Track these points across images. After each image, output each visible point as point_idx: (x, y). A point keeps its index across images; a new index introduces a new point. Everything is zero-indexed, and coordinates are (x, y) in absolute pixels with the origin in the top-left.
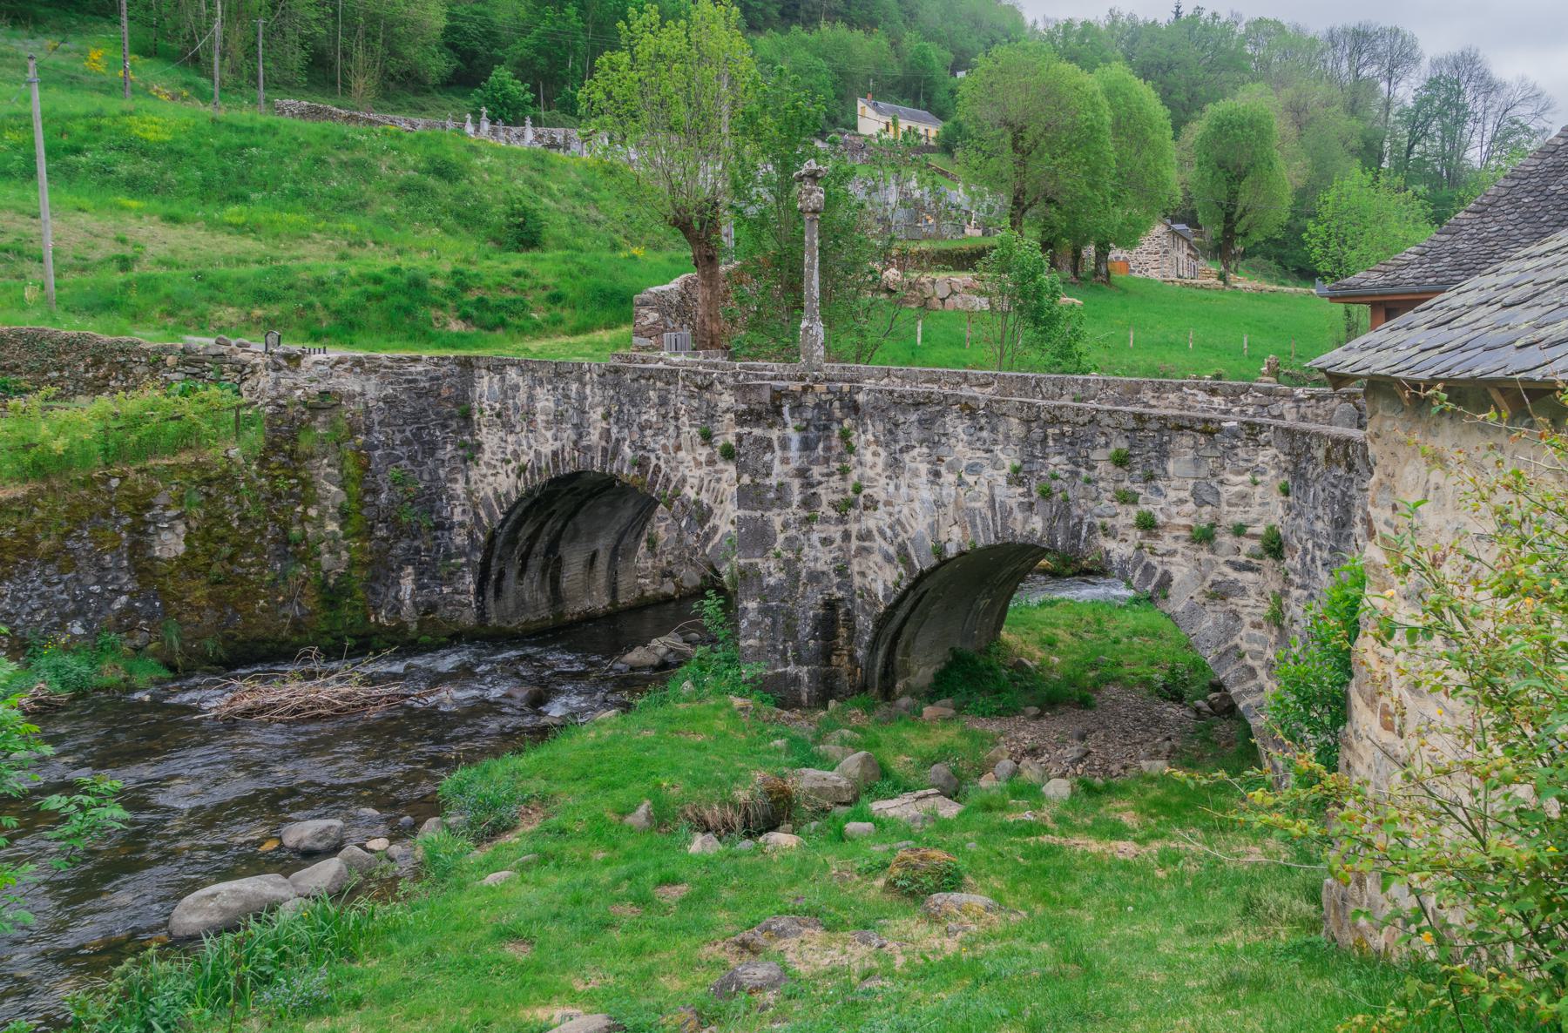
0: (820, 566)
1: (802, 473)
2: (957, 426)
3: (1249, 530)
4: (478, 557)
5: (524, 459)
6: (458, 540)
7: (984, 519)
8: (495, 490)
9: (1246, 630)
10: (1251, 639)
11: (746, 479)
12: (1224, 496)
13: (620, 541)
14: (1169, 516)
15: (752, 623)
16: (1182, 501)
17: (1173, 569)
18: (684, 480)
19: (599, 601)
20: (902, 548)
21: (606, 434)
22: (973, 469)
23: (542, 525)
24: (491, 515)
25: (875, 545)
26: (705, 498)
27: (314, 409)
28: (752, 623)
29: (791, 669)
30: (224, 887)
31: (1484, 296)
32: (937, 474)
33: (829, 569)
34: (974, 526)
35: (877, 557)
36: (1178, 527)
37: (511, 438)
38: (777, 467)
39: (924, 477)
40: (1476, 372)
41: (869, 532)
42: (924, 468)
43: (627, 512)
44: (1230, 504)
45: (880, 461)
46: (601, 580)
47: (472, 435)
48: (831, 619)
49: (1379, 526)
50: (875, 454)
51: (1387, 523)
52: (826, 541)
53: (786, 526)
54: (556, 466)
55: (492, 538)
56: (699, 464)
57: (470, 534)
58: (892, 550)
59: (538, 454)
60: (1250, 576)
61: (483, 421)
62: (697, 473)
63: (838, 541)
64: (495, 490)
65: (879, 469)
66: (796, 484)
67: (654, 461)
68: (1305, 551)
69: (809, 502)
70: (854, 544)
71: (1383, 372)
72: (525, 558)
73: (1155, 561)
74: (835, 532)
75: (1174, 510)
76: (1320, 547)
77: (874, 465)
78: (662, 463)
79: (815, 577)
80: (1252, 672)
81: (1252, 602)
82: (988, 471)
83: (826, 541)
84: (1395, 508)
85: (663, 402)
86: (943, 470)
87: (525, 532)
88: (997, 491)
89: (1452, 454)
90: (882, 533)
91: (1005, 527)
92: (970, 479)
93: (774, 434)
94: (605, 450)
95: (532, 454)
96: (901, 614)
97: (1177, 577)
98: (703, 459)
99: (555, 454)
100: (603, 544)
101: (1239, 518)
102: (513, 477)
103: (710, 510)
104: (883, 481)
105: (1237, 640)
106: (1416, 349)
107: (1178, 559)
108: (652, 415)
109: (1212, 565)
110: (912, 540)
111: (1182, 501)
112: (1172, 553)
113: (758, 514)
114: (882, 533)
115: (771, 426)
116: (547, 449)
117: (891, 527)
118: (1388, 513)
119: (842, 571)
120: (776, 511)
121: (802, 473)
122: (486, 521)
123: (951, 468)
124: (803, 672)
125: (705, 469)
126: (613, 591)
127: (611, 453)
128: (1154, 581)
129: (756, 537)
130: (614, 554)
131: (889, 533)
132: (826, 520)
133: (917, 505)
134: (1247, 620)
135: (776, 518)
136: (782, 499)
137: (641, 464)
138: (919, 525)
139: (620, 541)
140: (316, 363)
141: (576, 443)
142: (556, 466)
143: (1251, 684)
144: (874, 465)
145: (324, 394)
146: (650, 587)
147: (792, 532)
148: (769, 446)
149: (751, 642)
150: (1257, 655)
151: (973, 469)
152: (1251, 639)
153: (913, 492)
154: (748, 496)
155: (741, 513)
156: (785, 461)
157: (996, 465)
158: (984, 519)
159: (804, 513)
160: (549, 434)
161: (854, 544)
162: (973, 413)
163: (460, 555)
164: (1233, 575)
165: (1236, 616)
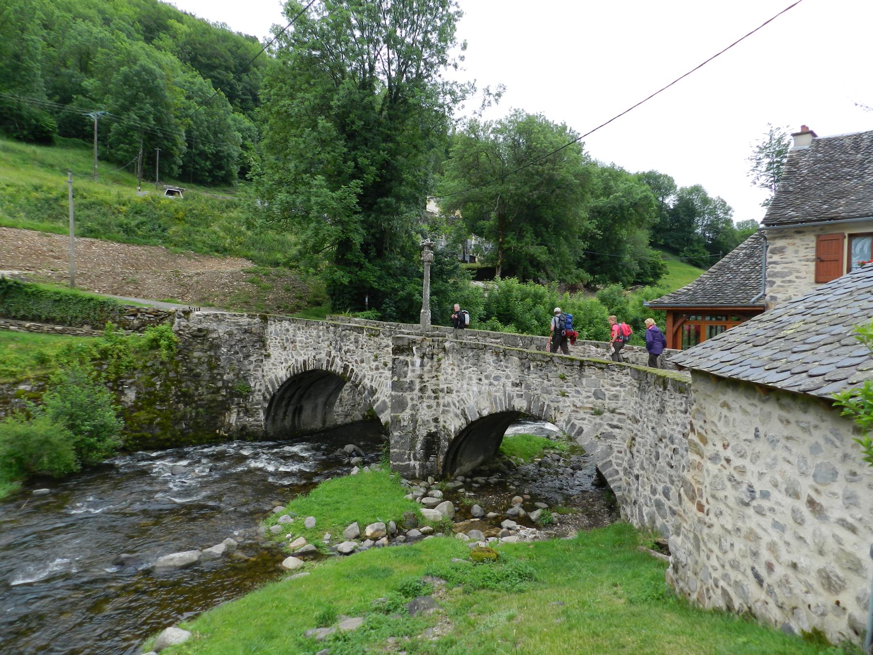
0: (426, 418)
1: (421, 377)
2: (489, 358)
3: (618, 411)
4: (266, 405)
5: (290, 363)
6: (257, 398)
7: (500, 400)
8: (276, 376)
9: (615, 454)
10: (617, 458)
11: (395, 379)
12: (607, 396)
13: (328, 399)
14: (583, 403)
15: (396, 442)
16: (589, 397)
17: (584, 427)
18: (365, 376)
19: (317, 425)
20: (463, 411)
21: (329, 354)
22: (497, 378)
23: (295, 393)
24: (273, 386)
25: (451, 410)
26: (374, 384)
27: (194, 337)
28: (396, 442)
29: (412, 462)
30: (177, 555)
31: (744, 338)
32: (480, 380)
33: (430, 419)
34: (496, 403)
35: (452, 415)
36: (586, 408)
37: (285, 353)
38: (410, 374)
39: (475, 381)
40: (750, 379)
41: (449, 403)
42: (474, 377)
43: (332, 387)
44: (610, 399)
45: (455, 373)
46: (319, 417)
47: (266, 350)
48: (431, 441)
49: (696, 427)
50: (452, 369)
51: (701, 427)
52: (429, 407)
53: (412, 399)
54: (305, 367)
55: (273, 397)
56: (371, 369)
57: (263, 394)
58: (459, 412)
59: (296, 361)
60: (617, 430)
61: (271, 344)
62: (370, 373)
63: (435, 407)
64: (276, 376)
65: (454, 376)
66: (417, 381)
67: (351, 367)
68: (644, 422)
69: (422, 390)
70: (441, 408)
71: (706, 370)
72: (287, 405)
73: (576, 422)
74: (433, 402)
75: (585, 400)
76: (651, 421)
77: (452, 374)
78: (354, 368)
79: (424, 423)
80: (617, 472)
81: (618, 442)
82: (503, 380)
83: (429, 407)
84: (705, 422)
85: (357, 341)
86: (483, 378)
87: (287, 395)
88: (507, 388)
89: (733, 405)
90: (454, 404)
91: (510, 404)
92: (496, 383)
93: (409, 359)
94: (328, 361)
95: (294, 361)
96: (461, 439)
97: (585, 430)
98: (374, 367)
99: (305, 361)
100: (321, 400)
101: (613, 405)
102: (284, 370)
103: (376, 390)
104: (456, 381)
105: (611, 458)
106: (718, 361)
107: (586, 422)
108: (352, 347)
109: (601, 425)
110: (468, 408)
111: (589, 397)
112: (584, 419)
113: (400, 394)
114: (454, 404)
115: (408, 355)
116: (301, 359)
117: (458, 402)
118: (702, 423)
119: (436, 420)
120: (408, 393)
121: (421, 377)
122: (271, 389)
123: (487, 377)
124: (417, 464)
125: (375, 372)
126: (324, 422)
127: (331, 363)
128: (575, 431)
129: (399, 404)
130: (325, 404)
131: (457, 404)
132: (429, 397)
133: (471, 393)
134: (616, 450)
135: (408, 395)
136: (411, 389)
137: (346, 368)
138: (471, 403)
139: (328, 399)
140: (198, 315)
141: (314, 357)
142: (305, 367)
143: (616, 477)
144: (452, 374)
145: (200, 330)
146: (340, 421)
147: (415, 402)
148: (407, 364)
149: (395, 450)
150: (619, 465)
151: (497, 378)
152: (617, 458)
153: (469, 387)
154: (395, 386)
155: (393, 393)
156: (413, 371)
157: (508, 377)
158: (500, 400)
159: (420, 394)
160: (302, 352)
161: (441, 408)
162: (497, 354)
163: (257, 404)
164: (610, 430)
165: (610, 447)
